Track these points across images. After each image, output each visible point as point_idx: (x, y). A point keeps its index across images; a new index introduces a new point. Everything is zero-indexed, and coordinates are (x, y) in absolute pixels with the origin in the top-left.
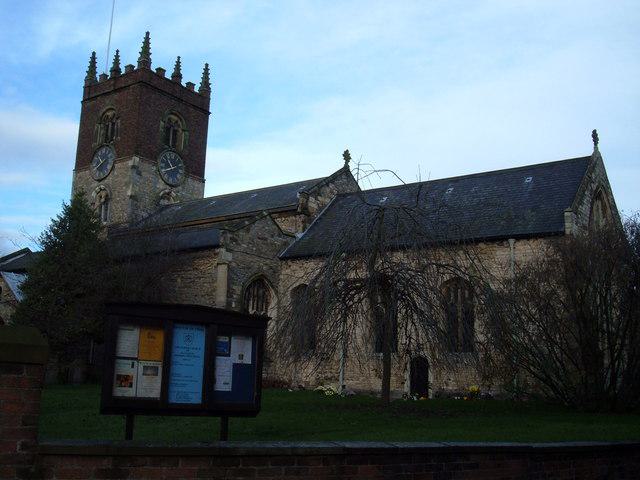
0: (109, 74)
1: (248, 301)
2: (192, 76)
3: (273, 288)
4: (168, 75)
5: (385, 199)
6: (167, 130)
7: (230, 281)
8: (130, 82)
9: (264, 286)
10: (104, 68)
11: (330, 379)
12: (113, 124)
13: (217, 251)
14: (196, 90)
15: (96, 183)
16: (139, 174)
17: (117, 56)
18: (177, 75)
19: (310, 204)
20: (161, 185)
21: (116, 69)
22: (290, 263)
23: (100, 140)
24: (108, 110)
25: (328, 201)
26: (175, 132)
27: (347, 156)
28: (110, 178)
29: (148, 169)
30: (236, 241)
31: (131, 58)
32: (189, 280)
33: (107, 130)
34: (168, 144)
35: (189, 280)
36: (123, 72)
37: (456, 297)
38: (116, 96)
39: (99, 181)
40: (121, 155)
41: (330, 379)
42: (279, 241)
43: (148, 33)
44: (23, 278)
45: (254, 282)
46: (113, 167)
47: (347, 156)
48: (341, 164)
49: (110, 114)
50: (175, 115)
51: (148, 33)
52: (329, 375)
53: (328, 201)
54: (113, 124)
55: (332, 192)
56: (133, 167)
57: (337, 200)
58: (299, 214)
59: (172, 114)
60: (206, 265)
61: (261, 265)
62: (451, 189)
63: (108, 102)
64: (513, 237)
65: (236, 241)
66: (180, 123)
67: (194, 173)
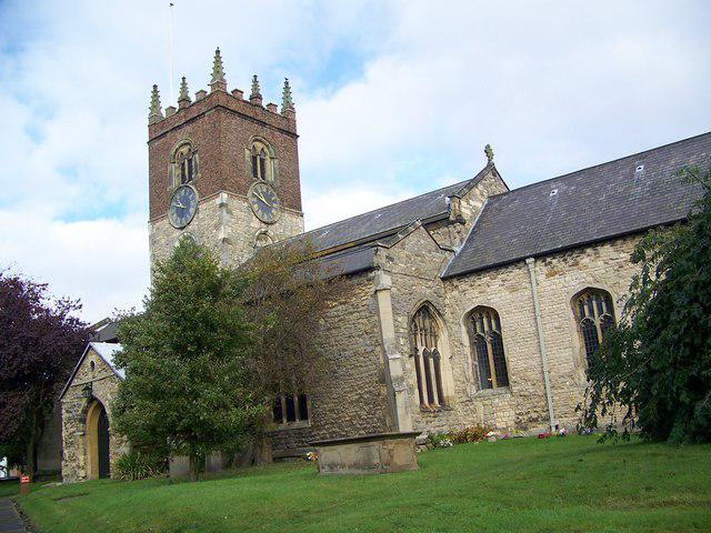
0: (177, 106)
1: (416, 334)
2: (271, 97)
3: (439, 314)
4: (246, 97)
5: (556, 191)
6: (254, 158)
7: (395, 311)
8: (204, 110)
9: (431, 317)
10: (170, 100)
11: (536, 420)
12: (190, 161)
13: (371, 275)
14: (279, 111)
15: (178, 233)
16: (229, 212)
17: (184, 84)
18: (256, 96)
19: (463, 210)
20: (255, 224)
21: (184, 99)
22: (456, 283)
23: (176, 182)
24: (182, 145)
25: (479, 205)
26: (262, 161)
27: (488, 151)
28: (195, 223)
29: (238, 206)
30: (392, 260)
31: (200, 83)
32: (337, 320)
33: (183, 170)
34: (255, 175)
35: (337, 320)
36: (193, 99)
37: (591, 311)
38: (189, 128)
39: (182, 228)
40: (206, 195)
41: (536, 420)
42: (439, 256)
43: (155, 87)
44: (118, 347)
45: (418, 311)
46: (197, 209)
47: (488, 151)
48: (484, 163)
49: (185, 150)
50: (260, 141)
51: (155, 87)
52: (534, 415)
53: (479, 205)
54: (190, 161)
55: (482, 195)
56: (222, 205)
57: (489, 204)
58: (453, 223)
59: (257, 140)
60: (363, 294)
61: (425, 291)
62: (556, 191)
63: (182, 136)
64: (537, 257)
65: (392, 260)
66: (266, 150)
67: (291, 206)
